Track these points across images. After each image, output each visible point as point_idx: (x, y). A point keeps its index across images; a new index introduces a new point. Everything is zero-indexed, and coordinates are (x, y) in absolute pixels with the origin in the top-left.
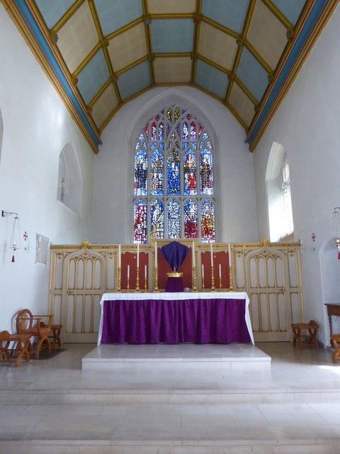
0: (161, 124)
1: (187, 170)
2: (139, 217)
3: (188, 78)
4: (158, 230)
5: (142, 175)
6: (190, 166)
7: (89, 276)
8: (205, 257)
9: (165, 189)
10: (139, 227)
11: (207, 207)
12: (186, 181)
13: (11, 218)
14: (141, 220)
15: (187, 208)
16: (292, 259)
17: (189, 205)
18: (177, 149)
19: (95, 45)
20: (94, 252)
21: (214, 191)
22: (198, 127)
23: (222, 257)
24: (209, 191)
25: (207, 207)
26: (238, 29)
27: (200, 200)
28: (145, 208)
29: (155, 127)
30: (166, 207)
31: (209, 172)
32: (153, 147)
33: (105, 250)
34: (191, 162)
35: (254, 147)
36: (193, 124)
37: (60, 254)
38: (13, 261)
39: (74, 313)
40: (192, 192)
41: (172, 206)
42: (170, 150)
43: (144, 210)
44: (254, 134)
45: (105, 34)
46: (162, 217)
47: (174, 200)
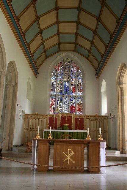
0: (62, 66)
1: (72, 85)
2: (52, 103)
3: (74, 49)
4: (60, 108)
5: (54, 86)
6: (73, 83)
8: (76, 119)
9: (63, 92)
10: (52, 107)
11: (79, 100)
12: (72, 89)
13: (20, 106)
14: (53, 104)
15: (71, 100)
16: (105, 121)
17: (72, 99)
18: (68, 76)
19: (29, 3)
20: (39, 117)
21: (83, 94)
22: (77, 67)
23: (81, 120)
24: (80, 94)
25: (79, 100)
26: (97, 14)
27: (76, 97)
28: (55, 100)
29: (60, 67)
30: (63, 99)
31: (81, 86)
32: (59, 75)
33: (43, 116)
34: (74, 81)
35: (98, 78)
36: (75, 66)
37: (28, 117)
38: (20, 118)
40: (74, 94)
41: (65, 99)
42: (66, 76)
43: (54, 100)
44: (98, 73)
45: (44, 39)
46: (61, 103)
47: (66, 97)
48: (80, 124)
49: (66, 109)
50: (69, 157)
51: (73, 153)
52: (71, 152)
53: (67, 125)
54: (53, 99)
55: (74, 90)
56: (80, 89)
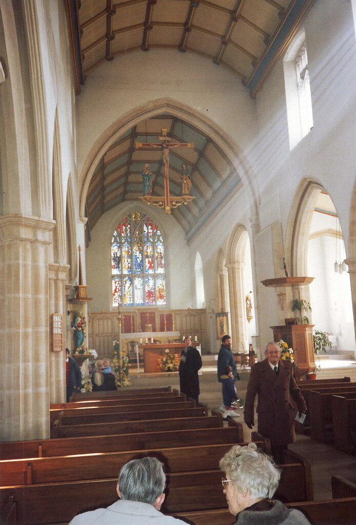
2: (116, 289)
7: (106, 327)
14: (117, 290)
21: (165, 271)
31: (162, 257)
36: (151, 225)
39: (100, 345)
41: (138, 282)
44: (189, 241)
46: (131, 288)
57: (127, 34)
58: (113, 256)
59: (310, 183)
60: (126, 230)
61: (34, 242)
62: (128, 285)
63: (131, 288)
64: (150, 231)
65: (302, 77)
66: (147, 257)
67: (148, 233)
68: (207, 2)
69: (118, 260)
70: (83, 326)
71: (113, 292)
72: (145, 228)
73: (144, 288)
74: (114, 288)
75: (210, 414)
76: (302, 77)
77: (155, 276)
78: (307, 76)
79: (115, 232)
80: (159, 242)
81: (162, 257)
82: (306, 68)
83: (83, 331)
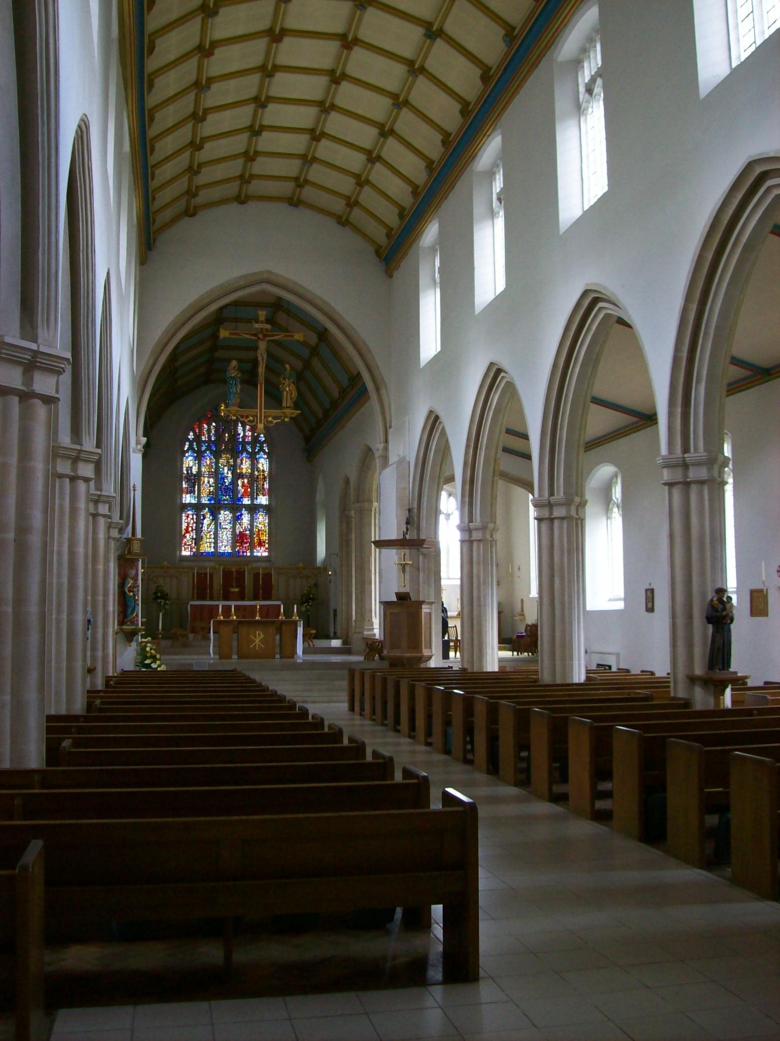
1: (241, 476)
2: (188, 527)
4: (208, 540)
5: (195, 480)
6: (244, 471)
8: (256, 576)
11: (261, 517)
14: (190, 529)
27: (253, 509)
31: (265, 478)
34: (246, 466)
41: (225, 516)
43: (193, 519)
48: (264, 588)
49: (225, 543)
50: (257, 641)
51: (262, 636)
52: (259, 635)
53: (237, 590)
54: (191, 516)
55: (246, 491)
56: (263, 488)
57: (236, 49)
58: (186, 472)
59: (596, 301)
60: (209, 431)
61: (73, 479)
62: (206, 522)
63: (213, 526)
64: (249, 433)
65: (589, 90)
66: (241, 476)
67: (245, 436)
68: (378, 2)
69: (195, 480)
70: (135, 590)
71: (184, 532)
72: (240, 429)
73: (234, 528)
74: (184, 526)
75: (398, 777)
76: (589, 90)
77: (253, 509)
78: (598, 89)
79: (191, 434)
80: (262, 453)
81: (265, 478)
82: (600, 74)
83: (135, 598)
